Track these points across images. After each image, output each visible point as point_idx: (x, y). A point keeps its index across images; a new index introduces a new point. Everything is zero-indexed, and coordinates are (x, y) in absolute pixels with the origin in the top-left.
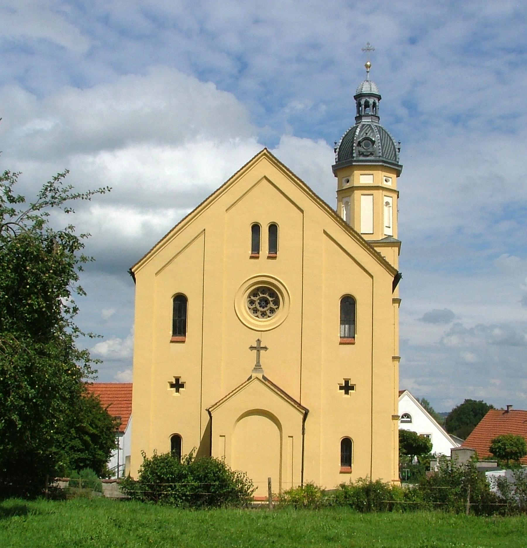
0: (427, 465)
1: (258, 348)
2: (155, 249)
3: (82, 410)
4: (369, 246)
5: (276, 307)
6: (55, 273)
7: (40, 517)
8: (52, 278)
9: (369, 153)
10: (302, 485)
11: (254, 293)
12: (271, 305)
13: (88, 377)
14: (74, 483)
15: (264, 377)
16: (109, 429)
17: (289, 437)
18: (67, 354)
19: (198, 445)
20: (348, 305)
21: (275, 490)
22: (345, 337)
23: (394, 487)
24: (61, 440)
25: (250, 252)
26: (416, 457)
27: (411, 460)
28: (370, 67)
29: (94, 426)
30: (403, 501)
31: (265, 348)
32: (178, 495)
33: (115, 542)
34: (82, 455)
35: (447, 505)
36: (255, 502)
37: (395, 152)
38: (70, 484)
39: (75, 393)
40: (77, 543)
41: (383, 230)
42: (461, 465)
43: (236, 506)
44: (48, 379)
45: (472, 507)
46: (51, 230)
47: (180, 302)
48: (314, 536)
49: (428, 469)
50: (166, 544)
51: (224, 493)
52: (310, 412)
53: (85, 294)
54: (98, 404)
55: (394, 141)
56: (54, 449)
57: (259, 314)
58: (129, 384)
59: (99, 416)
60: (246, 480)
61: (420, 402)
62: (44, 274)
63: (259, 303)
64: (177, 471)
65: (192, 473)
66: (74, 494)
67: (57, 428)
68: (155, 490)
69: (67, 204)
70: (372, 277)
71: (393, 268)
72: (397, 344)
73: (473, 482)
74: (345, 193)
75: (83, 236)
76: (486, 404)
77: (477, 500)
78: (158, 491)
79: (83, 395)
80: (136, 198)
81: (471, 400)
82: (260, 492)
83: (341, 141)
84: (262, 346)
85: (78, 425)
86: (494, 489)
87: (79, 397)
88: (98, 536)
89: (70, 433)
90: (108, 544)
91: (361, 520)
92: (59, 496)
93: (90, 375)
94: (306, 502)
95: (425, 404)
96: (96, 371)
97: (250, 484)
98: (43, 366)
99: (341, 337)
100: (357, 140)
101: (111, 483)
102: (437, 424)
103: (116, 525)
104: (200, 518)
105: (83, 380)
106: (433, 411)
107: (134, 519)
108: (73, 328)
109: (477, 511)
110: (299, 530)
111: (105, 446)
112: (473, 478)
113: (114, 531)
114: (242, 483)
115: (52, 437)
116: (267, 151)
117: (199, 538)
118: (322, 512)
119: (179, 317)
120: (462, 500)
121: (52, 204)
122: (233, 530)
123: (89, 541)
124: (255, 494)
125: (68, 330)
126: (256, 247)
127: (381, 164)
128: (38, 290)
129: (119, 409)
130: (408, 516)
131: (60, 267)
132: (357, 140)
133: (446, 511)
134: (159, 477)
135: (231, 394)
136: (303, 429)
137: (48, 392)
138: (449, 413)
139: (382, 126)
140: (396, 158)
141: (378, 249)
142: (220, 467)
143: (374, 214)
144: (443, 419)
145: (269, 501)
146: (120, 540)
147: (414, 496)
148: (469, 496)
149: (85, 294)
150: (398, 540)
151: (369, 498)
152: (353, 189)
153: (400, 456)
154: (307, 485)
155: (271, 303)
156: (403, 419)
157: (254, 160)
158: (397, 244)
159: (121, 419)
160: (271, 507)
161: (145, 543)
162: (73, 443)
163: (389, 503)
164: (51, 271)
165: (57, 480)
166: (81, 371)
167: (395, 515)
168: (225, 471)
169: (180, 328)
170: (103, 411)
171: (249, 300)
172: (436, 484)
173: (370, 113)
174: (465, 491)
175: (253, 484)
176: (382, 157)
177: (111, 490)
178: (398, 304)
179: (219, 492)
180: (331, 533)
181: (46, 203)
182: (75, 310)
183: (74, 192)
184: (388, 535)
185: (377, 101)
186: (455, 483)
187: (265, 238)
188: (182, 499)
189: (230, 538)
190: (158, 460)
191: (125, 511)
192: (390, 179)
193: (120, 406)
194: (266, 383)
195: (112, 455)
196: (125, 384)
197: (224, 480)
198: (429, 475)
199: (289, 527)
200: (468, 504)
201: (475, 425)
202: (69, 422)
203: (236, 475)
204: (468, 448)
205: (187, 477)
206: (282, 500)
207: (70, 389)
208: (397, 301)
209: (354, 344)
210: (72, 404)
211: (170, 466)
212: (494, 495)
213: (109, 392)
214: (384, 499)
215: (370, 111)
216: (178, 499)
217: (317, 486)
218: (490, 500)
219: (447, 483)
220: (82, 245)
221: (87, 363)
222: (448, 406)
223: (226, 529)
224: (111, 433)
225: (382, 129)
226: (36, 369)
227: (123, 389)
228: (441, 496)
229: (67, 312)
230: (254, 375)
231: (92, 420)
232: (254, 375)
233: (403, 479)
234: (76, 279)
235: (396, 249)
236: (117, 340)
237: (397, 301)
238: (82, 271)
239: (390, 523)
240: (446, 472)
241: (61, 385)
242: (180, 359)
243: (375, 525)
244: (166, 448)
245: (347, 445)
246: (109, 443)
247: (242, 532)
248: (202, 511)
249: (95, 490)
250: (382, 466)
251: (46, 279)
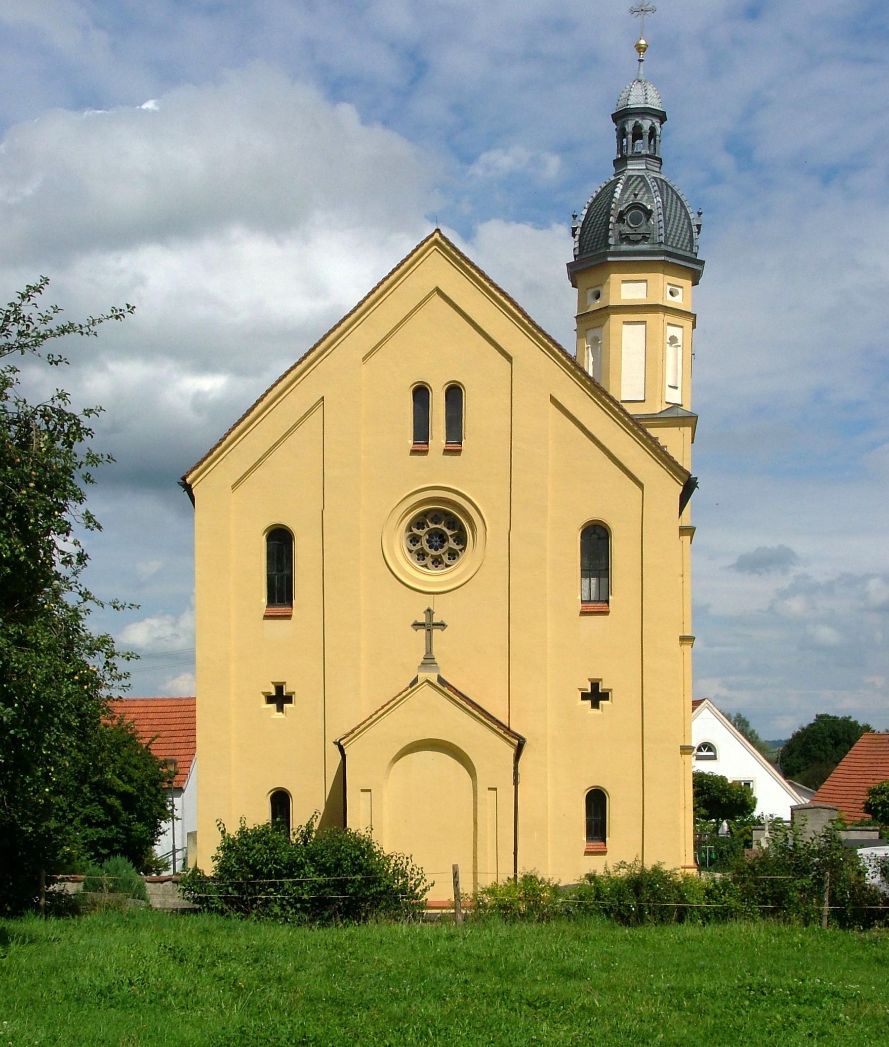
0: (747, 836)
1: (429, 625)
2: (229, 438)
3: (103, 749)
4: (637, 426)
5: (461, 547)
6: (39, 487)
7: (33, 947)
8: (34, 497)
9: (639, 237)
10: (516, 876)
11: (419, 522)
12: (451, 544)
13: (109, 687)
14: (94, 884)
15: (441, 680)
16: (154, 783)
17: (489, 789)
18: (70, 645)
19: (322, 809)
20: (596, 541)
21: (466, 887)
22: (590, 601)
23: (686, 878)
24: (64, 805)
25: (411, 442)
26: (725, 824)
27: (716, 829)
28: (645, 50)
29: (126, 779)
30: (704, 904)
31: (442, 625)
32: (287, 901)
33: (174, 989)
34: (103, 833)
35: (786, 909)
36: (430, 911)
37: (691, 233)
38: (85, 887)
39: (87, 718)
40: (105, 992)
41: (662, 396)
42: (813, 836)
43: (395, 918)
44: (37, 691)
45: (834, 914)
46: (25, 402)
47: (280, 542)
48: (540, 970)
49: (748, 844)
50: (268, 991)
51: (372, 895)
52: (528, 741)
53: (99, 527)
54: (132, 737)
55: (689, 210)
56: (53, 824)
57: (428, 561)
58: (189, 699)
59: (134, 761)
60: (412, 869)
61: (732, 720)
62: (18, 488)
63: (428, 541)
64: (286, 857)
65: (312, 859)
66: (94, 904)
67: (57, 784)
68: (244, 893)
69: (49, 346)
70: (641, 485)
71: (681, 468)
72: (688, 612)
73: (834, 867)
74: (593, 320)
75: (88, 412)
76: (856, 722)
77: (843, 900)
78: (250, 894)
79: (103, 721)
80: (197, 349)
81: (827, 716)
82: (439, 893)
83: (585, 212)
84: (435, 621)
85: (96, 779)
86: (873, 879)
87: (96, 724)
88: (143, 979)
89: (82, 792)
90: (161, 992)
91: (626, 940)
92: (65, 908)
93: (116, 683)
94: (523, 907)
95: (741, 725)
96: (127, 675)
97: (419, 877)
98: (25, 666)
99: (583, 602)
100: (617, 208)
101: (162, 882)
102: (765, 761)
103: (175, 958)
104: (329, 941)
105: (103, 693)
106: (757, 738)
107: (208, 946)
108: (80, 594)
109: (842, 919)
110: (511, 958)
111: (148, 814)
112: (834, 859)
113: (172, 968)
114: (404, 875)
115: (47, 800)
116: (441, 235)
117: (328, 977)
118: (553, 924)
119: (278, 571)
120: (814, 900)
121: (22, 347)
122: (390, 962)
123: (125, 988)
124: (430, 897)
125: (70, 598)
126: (421, 432)
127: (662, 258)
128: (10, 522)
129: (171, 746)
130: (713, 930)
131: (48, 475)
132: (617, 208)
133: (784, 921)
134: (252, 868)
135: (380, 713)
136: (516, 774)
137: (38, 714)
138: (786, 741)
139: (667, 180)
140: (692, 246)
141: (653, 432)
142: (363, 849)
143: (646, 362)
144: (776, 752)
145: (455, 908)
146: (184, 984)
147: (724, 894)
148: (827, 893)
149: (99, 527)
150: (697, 974)
151: (638, 900)
152: (608, 311)
153: (696, 822)
154: (525, 876)
155: (451, 540)
156: (701, 754)
157: (415, 255)
158: (689, 420)
159: (176, 764)
160: (460, 918)
161: (230, 990)
162: (88, 810)
163: (678, 907)
164: (32, 485)
165: (62, 880)
166: (98, 676)
167: (689, 930)
168: (372, 855)
169: (280, 591)
170: (142, 750)
171: (410, 536)
172: (766, 870)
173: (643, 152)
174: (820, 883)
175: (425, 877)
176: (666, 244)
177: (162, 896)
178: (689, 537)
179: (364, 894)
180: (574, 962)
181: (10, 347)
182: (82, 558)
183: (59, 320)
184: (678, 965)
185: (657, 125)
186: (801, 870)
187: (438, 413)
188: (296, 908)
189: (387, 977)
190: (250, 837)
191: (190, 932)
192: (680, 290)
193: (174, 739)
194: (445, 689)
195: (161, 831)
196: (180, 699)
197: (371, 872)
198: (750, 855)
199: (494, 954)
200: (826, 908)
201: (837, 763)
202: (80, 773)
203: (393, 862)
204: (823, 805)
205: (303, 868)
206: (479, 905)
207: (78, 709)
208: (687, 531)
209: (606, 613)
210: (83, 737)
211: (274, 848)
212: (875, 891)
213: (151, 716)
214: (669, 901)
215: (641, 146)
216: (288, 908)
217: (543, 879)
218: (866, 900)
219: (786, 869)
220: (88, 432)
221: (109, 660)
222: (785, 728)
223: (378, 960)
224: (158, 791)
225: (667, 185)
226: (13, 672)
227: (178, 709)
228: (774, 893)
229: (66, 562)
230: (422, 676)
231: (122, 768)
232: (422, 676)
233: (702, 864)
234: (80, 499)
235: (688, 430)
236: (162, 614)
237: (687, 531)
238: (92, 482)
239: (681, 943)
240: (784, 849)
241: (62, 702)
242: (284, 648)
243: (654, 947)
244: (261, 815)
245: (596, 801)
246: (156, 809)
247: (407, 965)
248: (332, 929)
249: (134, 897)
250: (662, 839)
251: (22, 499)
